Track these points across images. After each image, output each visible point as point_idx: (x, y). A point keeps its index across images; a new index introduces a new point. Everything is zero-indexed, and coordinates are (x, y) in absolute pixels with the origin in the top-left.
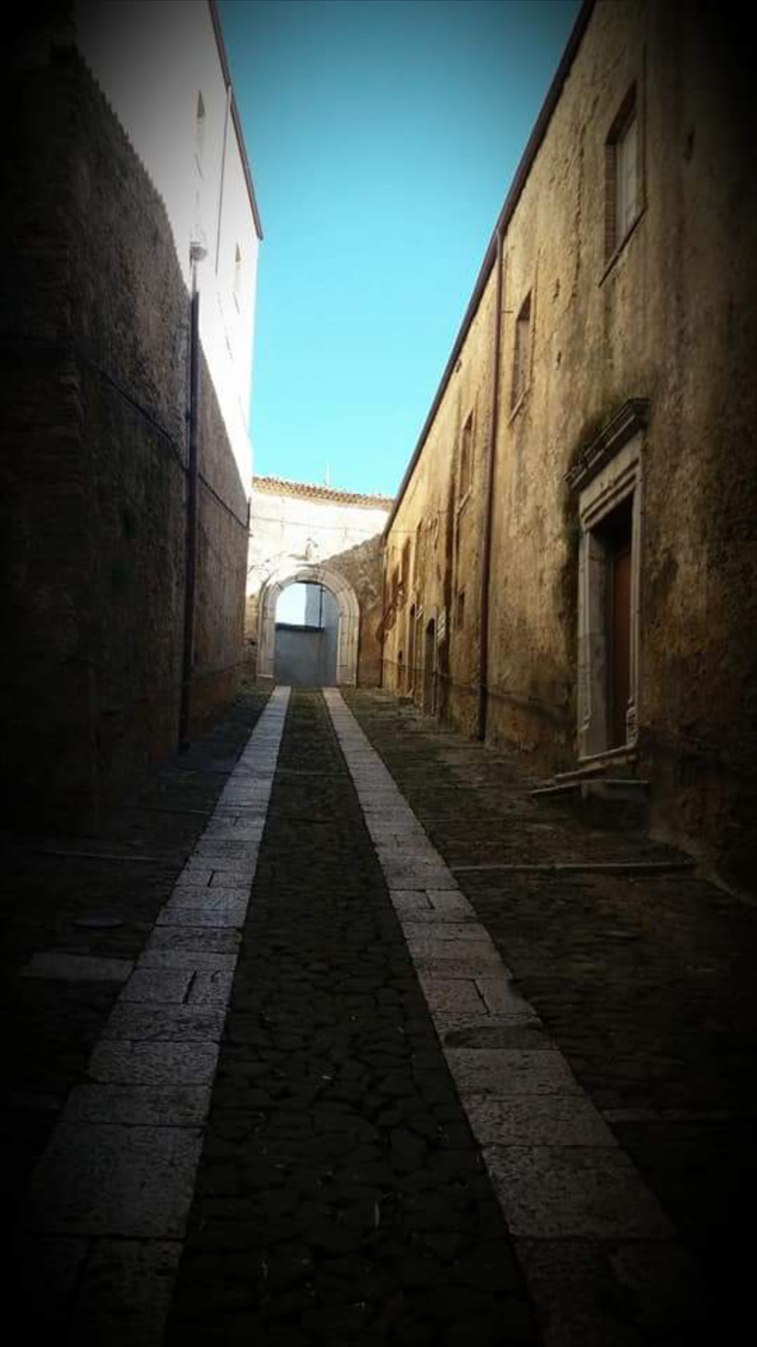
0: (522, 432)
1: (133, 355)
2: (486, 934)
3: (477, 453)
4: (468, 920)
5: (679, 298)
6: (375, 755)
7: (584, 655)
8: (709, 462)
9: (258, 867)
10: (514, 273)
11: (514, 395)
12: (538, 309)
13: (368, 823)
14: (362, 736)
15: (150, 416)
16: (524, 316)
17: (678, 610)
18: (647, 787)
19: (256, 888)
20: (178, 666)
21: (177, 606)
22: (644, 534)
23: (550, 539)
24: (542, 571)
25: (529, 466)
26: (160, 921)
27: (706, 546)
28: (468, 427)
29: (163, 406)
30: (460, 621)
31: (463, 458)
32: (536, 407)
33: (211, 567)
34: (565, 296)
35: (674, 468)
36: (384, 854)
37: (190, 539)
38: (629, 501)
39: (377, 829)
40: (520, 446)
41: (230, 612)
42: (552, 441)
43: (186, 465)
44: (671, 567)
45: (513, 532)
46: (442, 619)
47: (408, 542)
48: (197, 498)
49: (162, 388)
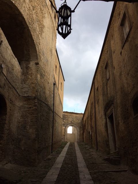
0: (98, 104)
1: (45, 97)
2: (93, 182)
3: (93, 107)
4: (90, 180)
5: (115, 87)
6: (81, 153)
7: (110, 136)
8: (121, 108)
9: (60, 172)
10: (96, 84)
11: (97, 100)
12: (99, 88)
13: (78, 164)
14: (79, 150)
15: (47, 105)
16: (97, 90)
17: (121, 130)
18: (120, 157)
19: (59, 175)
20: (51, 140)
21: (51, 130)
22: (115, 118)
23: (103, 119)
24: (103, 124)
25: (100, 109)
26: (43, 180)
27: (123, 120)
28: (92, 104)
29: (49, 103)
30: (93, 131)
31: (91, 108)
32: (100, 101)
33: (57, 125)
34: (102, 87)
35: (117, 109)
36: (79, 169)
37: (53, 121)
38: (112, 114)
39: (79, 165)
40: (98, 107)
41: (60, 131)
42: (102, 106)
43: (53, 111)
44: (119, 123)
45: (99, 118)
46: (91, 131)
47: (86, 120)
48: (54, 115)
49: (49, 101)
